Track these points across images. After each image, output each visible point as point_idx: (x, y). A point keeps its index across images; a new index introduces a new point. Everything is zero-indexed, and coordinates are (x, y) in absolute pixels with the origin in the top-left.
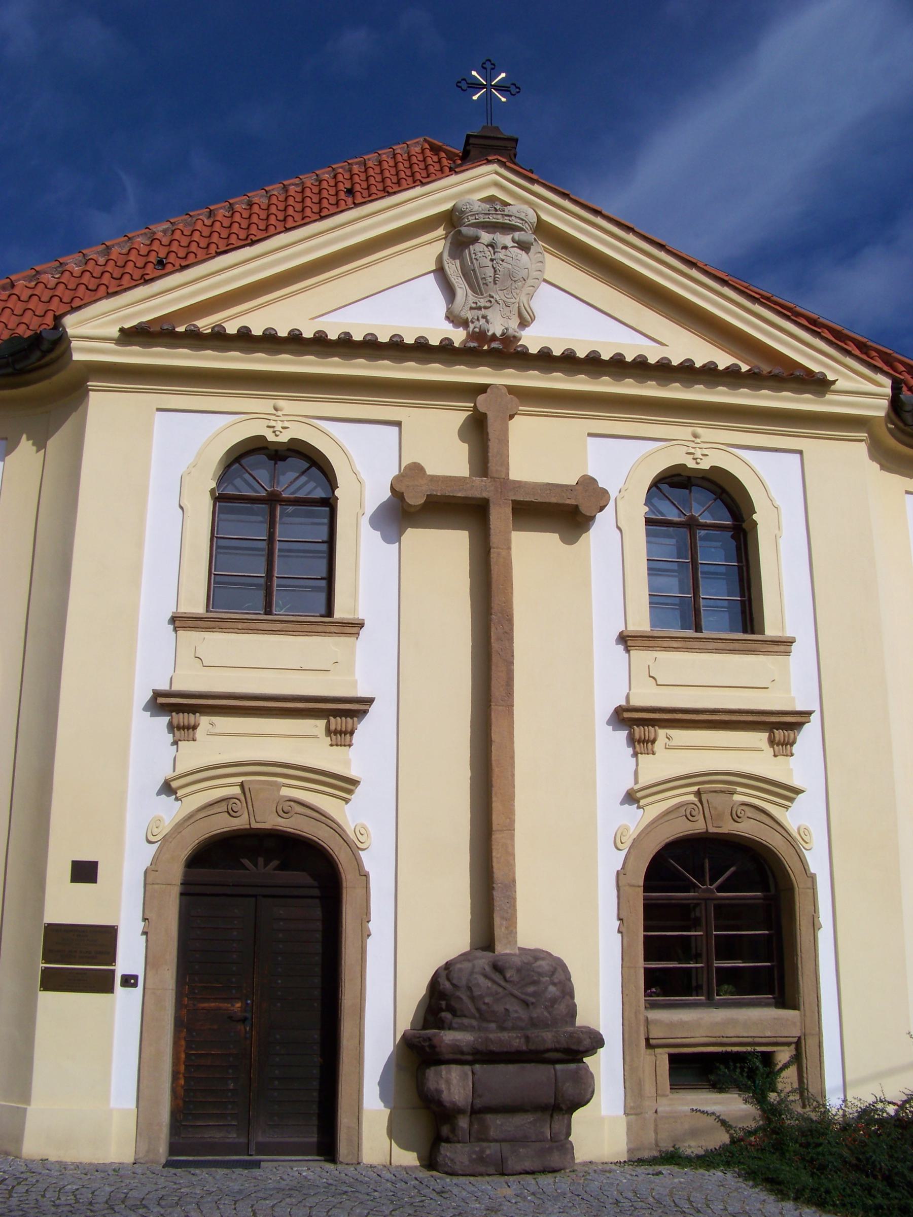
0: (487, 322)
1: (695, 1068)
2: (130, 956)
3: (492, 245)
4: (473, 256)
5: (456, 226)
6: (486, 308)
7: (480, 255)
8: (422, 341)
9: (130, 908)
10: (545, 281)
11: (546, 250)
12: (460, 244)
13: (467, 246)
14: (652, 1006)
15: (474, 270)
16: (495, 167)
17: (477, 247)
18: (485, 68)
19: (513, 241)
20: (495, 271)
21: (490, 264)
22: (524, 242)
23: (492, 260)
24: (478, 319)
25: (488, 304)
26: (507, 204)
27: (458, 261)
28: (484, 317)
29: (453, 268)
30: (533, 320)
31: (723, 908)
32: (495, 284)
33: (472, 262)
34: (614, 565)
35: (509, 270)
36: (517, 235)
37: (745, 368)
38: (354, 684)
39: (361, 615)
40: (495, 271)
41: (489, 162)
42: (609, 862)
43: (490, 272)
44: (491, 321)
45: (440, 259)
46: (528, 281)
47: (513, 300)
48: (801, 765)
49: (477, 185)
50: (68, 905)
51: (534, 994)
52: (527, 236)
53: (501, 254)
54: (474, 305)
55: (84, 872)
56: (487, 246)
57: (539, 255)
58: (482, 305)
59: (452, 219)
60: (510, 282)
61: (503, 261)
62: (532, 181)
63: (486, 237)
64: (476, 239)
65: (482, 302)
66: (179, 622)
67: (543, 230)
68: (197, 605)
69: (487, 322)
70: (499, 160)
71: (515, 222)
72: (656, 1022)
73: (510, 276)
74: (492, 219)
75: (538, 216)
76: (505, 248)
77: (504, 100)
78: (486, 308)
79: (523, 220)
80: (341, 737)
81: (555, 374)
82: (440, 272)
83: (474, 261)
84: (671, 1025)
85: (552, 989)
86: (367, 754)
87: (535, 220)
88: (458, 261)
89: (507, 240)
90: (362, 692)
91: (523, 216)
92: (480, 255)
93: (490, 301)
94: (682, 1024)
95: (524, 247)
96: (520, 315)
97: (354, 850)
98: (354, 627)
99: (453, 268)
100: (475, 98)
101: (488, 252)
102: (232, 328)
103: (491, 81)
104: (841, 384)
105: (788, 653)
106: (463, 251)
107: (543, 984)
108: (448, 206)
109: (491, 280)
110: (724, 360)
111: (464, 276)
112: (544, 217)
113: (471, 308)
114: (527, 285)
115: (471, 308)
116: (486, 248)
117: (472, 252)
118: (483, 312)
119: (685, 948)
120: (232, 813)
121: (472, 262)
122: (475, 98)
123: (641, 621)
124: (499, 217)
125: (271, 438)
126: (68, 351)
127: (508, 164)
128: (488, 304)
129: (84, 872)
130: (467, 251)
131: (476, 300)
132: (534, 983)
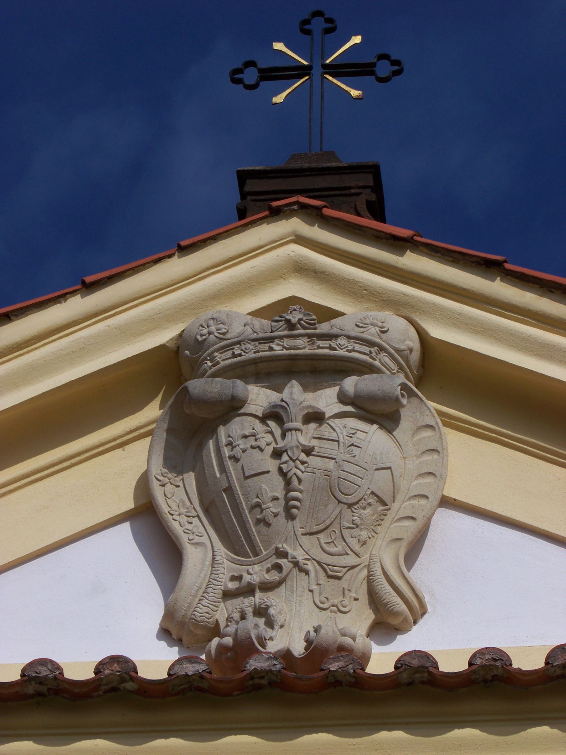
0: (270, 624)
3: (275, 415)
4: (226, 452)
5: (186, 395)
6: (267, 587)
7: (242, 444)
8: (44, 672)
10: (446, 502)
11: (450, 422)
12: (192, 430)
13: (213, 432)
15: (229, 490)
16: (295, 224)
17: (238, 427)
18: (308, 32)
19: (343, 398)
20: (288, 482)
21: (272, 465)
22: (373, 398)
23: (277, 454)
24: (243, 617)
25: (274, 576)
26: (331, 314)
27: (190, 478)
28: (261, 612)
29: (177, 500)
30: (423, 614)
32: (291, 517)
33: (223, 469)
35: (327, 474)
36: (350, 384)
40: (288, 482)
41: (276, 214)
43: (273, 486)
44: (280, 620)
45: (143, 486)
46: (395, 506)
47: (351, 560)
49: (247, 275)
52: (391, 382)
53: (306, 435)
54: (232, 585)
56: (263, 419)
57: (428, 433)
58: (256, 579)
59: (169, 370)
60: (333, 509)
61: (308, 451)
62: (398, 244)
63: (259, 397)
64: (233, 407)
65: (257, 573)
67: (441, 372)
69: (270, 624)
70: (304, 207)
71: (343, 349)
73: (336, 492)
75: (422, 335)
76: (315, 417)
77: (355, 93)
78: (267, 587)
79: (370, 344)
81: (457, 733)
82: (145, 515)
83: (229, 464)
87: (414, 342)
88: (190, 478)
89: (326, 399)
91: (371, 334)
92: (242, 444)
93: (278, 567)
95: (381, 413)
96: (375, 600)
99: (177, 500)
100: (279, 99)
101: (267, 436)
103: (324, 58)
106: (201, 446)
108: (165, 336)
109: (277, 508)
111: (207, 510)
112: (437, 332)
113: (227, 595)
114: (391, 515)
115: (227, 595)
116: (259, 427)
117: (224, 441)
118: (259, 597)
121: (223, 469)
122: (279, 99)
124: (300, 342)
127: (327, 212)
128: (274, 576)
130: (211, 444)
131: (238, 570)
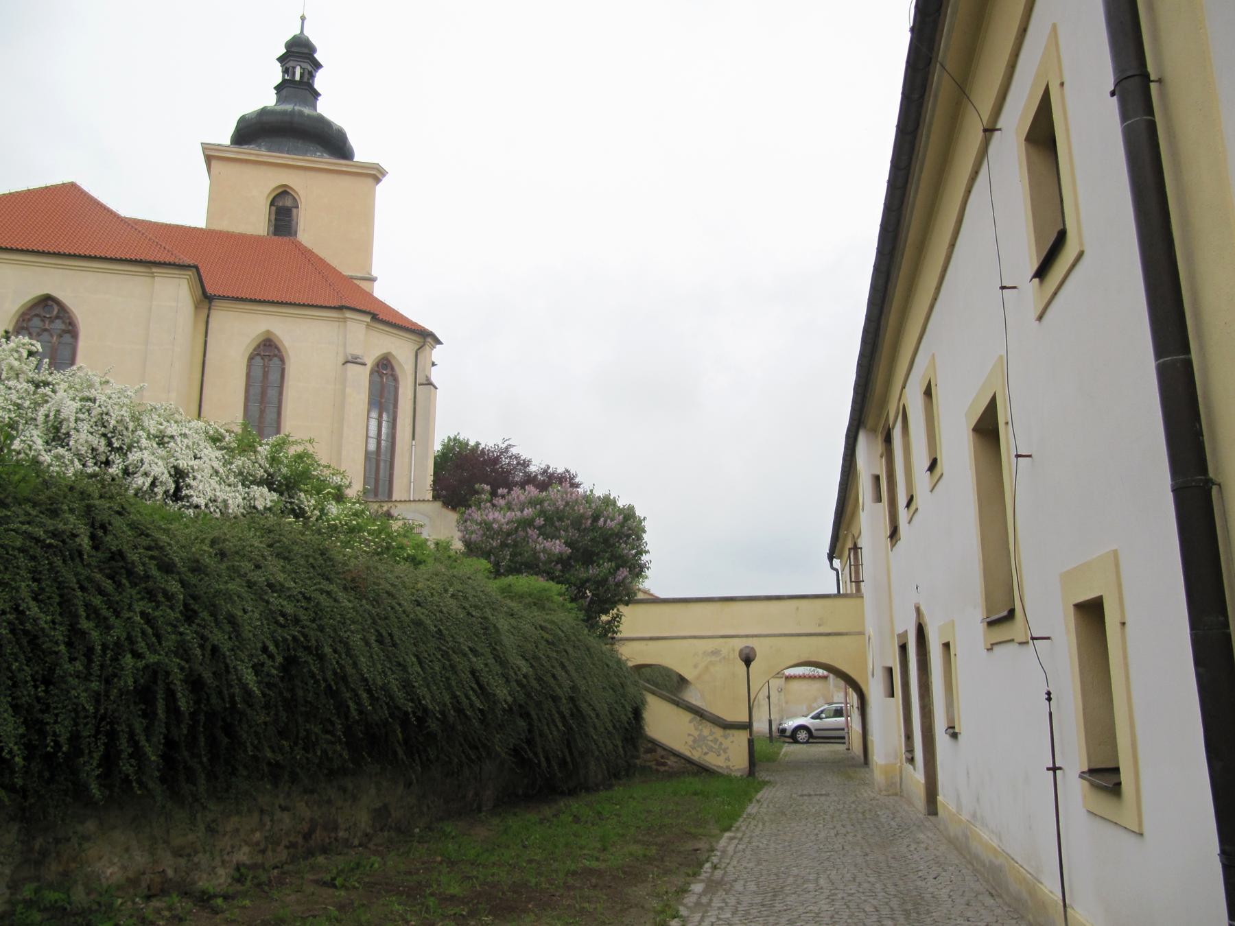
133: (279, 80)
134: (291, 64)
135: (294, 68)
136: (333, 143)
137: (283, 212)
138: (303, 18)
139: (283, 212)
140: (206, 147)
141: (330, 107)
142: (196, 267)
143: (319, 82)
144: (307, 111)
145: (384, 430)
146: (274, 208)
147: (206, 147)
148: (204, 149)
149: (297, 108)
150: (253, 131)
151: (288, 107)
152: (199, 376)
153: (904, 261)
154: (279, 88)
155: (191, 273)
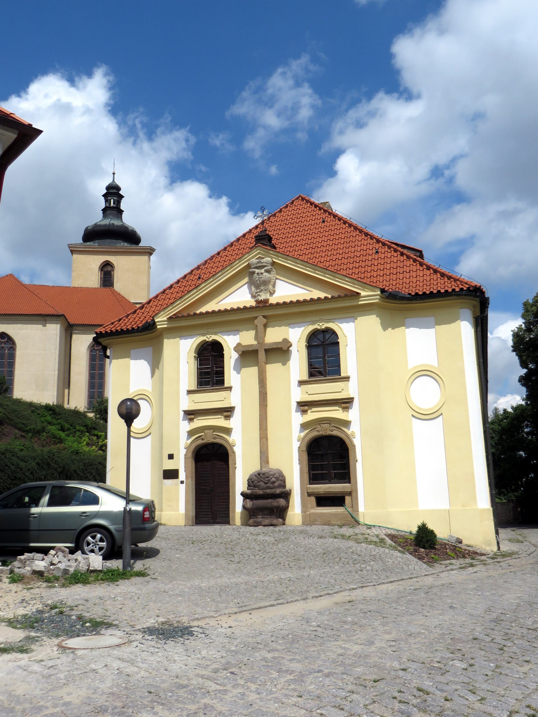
1: (323, 500)
2: (182, 475)
9: (181, 464)
14: (310, 484)
31: (329, 456)
34: (298, 362)
36: (266, 268)
37: (330, 296)
38: (231, 403)
39: (349, 374)
42: (296, 445)
48: (351, 415)
50: (169, 465)
51: (268, 480)
55: (171, 457)
63: (257, 271)
66: (190, 392)
68: (194, 387)
71: (264, 264)
72: (309, 487)
74: (258, 265)
80: (228, 417)
84: (313, 488)
85: (273, 479)
86: (234, 423)
89: (263, 271)
90: (232, 406)
94: (316, 488)
97: (232, 446)
98: (347, 378)
102: (192, 313)
104: (363, 293)
105: (348, 381)
107: (280, 479)
110: (322, 295)
112: (274, 260)
119: (322, 467)
120: (203, 439)
123: (194, 387)
125: (207, 340)
126: (156, 327)
129: (171, 457)
132: (268, 477)
133: (104, 206)
134: (109, 198)
135: (110, 200)
136: (130, 237)
137: (107, 272)
138: (114, 174)
139: (107, 272)
140: (70, 246)
141: (130, 219)
142: (63, 315)
143: (123, 206)
144: (116, 222)
145: (179, 302)
146: (102, 272)
147: (70, 246)
148: (69, 247)
149: (112, 222)
150: (93, 235)
151: (107, 222)
152: (68, 360)
153: (335, 509)
154: (104, 210)
155: (62, 318)
